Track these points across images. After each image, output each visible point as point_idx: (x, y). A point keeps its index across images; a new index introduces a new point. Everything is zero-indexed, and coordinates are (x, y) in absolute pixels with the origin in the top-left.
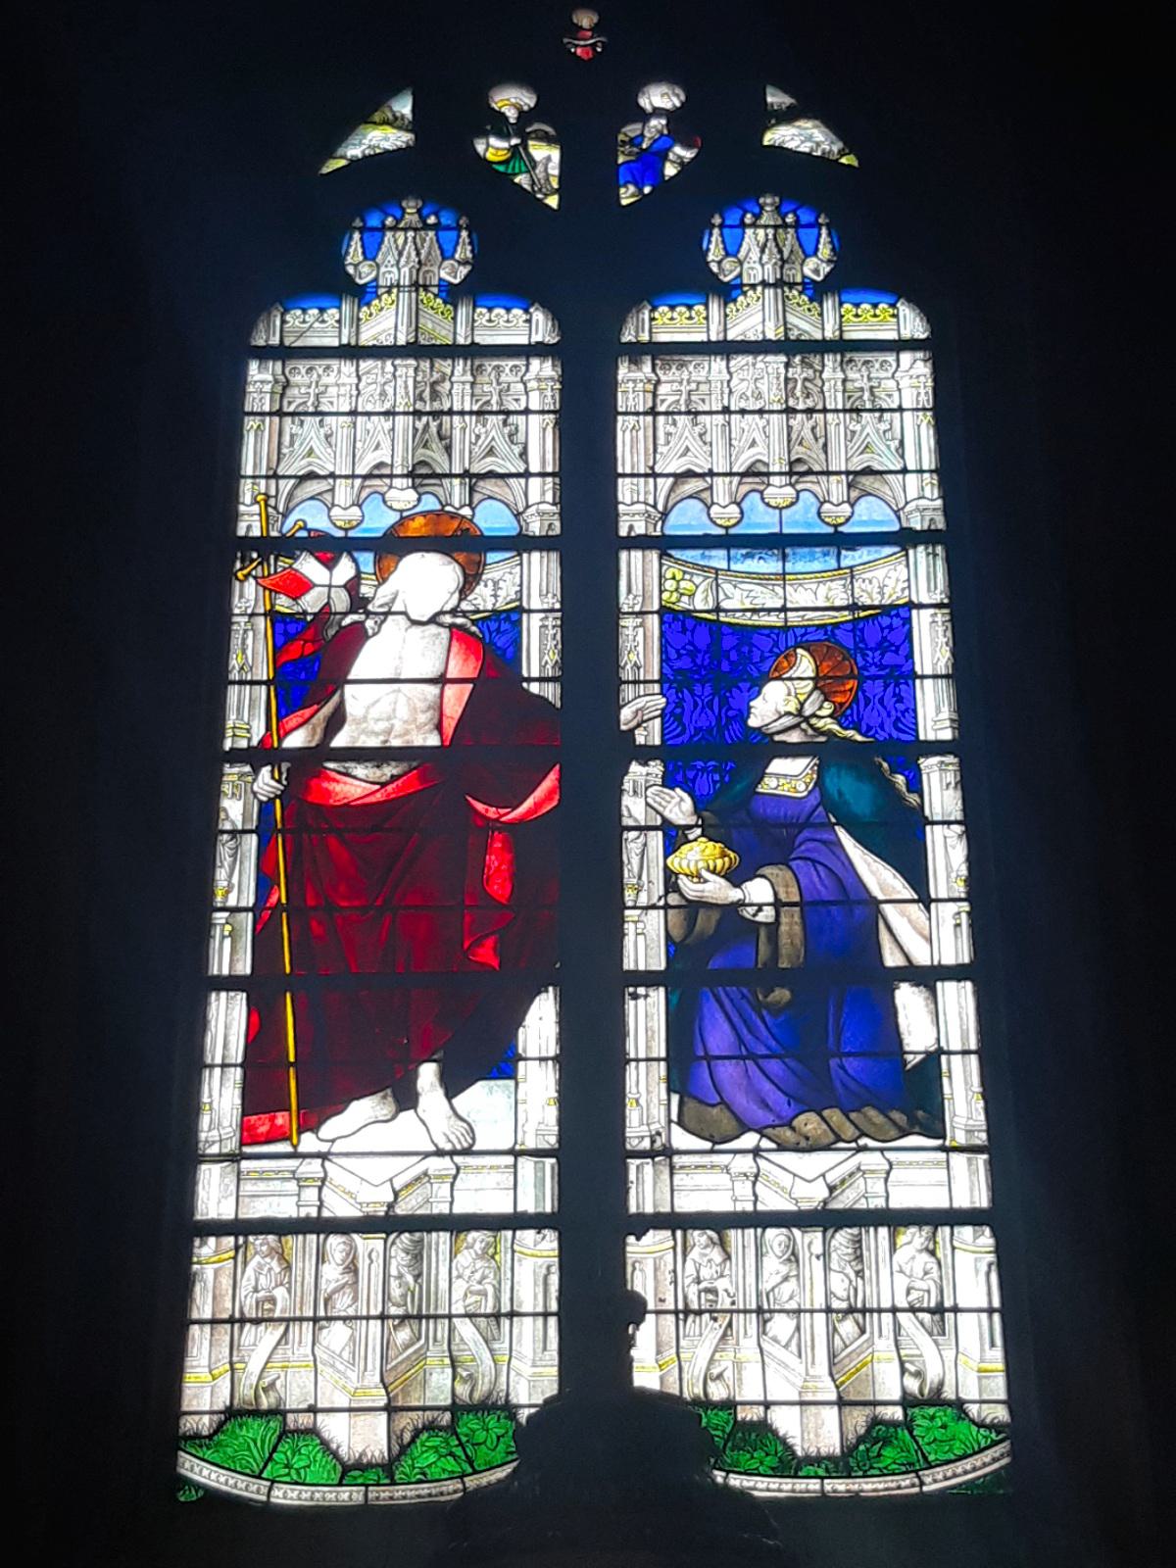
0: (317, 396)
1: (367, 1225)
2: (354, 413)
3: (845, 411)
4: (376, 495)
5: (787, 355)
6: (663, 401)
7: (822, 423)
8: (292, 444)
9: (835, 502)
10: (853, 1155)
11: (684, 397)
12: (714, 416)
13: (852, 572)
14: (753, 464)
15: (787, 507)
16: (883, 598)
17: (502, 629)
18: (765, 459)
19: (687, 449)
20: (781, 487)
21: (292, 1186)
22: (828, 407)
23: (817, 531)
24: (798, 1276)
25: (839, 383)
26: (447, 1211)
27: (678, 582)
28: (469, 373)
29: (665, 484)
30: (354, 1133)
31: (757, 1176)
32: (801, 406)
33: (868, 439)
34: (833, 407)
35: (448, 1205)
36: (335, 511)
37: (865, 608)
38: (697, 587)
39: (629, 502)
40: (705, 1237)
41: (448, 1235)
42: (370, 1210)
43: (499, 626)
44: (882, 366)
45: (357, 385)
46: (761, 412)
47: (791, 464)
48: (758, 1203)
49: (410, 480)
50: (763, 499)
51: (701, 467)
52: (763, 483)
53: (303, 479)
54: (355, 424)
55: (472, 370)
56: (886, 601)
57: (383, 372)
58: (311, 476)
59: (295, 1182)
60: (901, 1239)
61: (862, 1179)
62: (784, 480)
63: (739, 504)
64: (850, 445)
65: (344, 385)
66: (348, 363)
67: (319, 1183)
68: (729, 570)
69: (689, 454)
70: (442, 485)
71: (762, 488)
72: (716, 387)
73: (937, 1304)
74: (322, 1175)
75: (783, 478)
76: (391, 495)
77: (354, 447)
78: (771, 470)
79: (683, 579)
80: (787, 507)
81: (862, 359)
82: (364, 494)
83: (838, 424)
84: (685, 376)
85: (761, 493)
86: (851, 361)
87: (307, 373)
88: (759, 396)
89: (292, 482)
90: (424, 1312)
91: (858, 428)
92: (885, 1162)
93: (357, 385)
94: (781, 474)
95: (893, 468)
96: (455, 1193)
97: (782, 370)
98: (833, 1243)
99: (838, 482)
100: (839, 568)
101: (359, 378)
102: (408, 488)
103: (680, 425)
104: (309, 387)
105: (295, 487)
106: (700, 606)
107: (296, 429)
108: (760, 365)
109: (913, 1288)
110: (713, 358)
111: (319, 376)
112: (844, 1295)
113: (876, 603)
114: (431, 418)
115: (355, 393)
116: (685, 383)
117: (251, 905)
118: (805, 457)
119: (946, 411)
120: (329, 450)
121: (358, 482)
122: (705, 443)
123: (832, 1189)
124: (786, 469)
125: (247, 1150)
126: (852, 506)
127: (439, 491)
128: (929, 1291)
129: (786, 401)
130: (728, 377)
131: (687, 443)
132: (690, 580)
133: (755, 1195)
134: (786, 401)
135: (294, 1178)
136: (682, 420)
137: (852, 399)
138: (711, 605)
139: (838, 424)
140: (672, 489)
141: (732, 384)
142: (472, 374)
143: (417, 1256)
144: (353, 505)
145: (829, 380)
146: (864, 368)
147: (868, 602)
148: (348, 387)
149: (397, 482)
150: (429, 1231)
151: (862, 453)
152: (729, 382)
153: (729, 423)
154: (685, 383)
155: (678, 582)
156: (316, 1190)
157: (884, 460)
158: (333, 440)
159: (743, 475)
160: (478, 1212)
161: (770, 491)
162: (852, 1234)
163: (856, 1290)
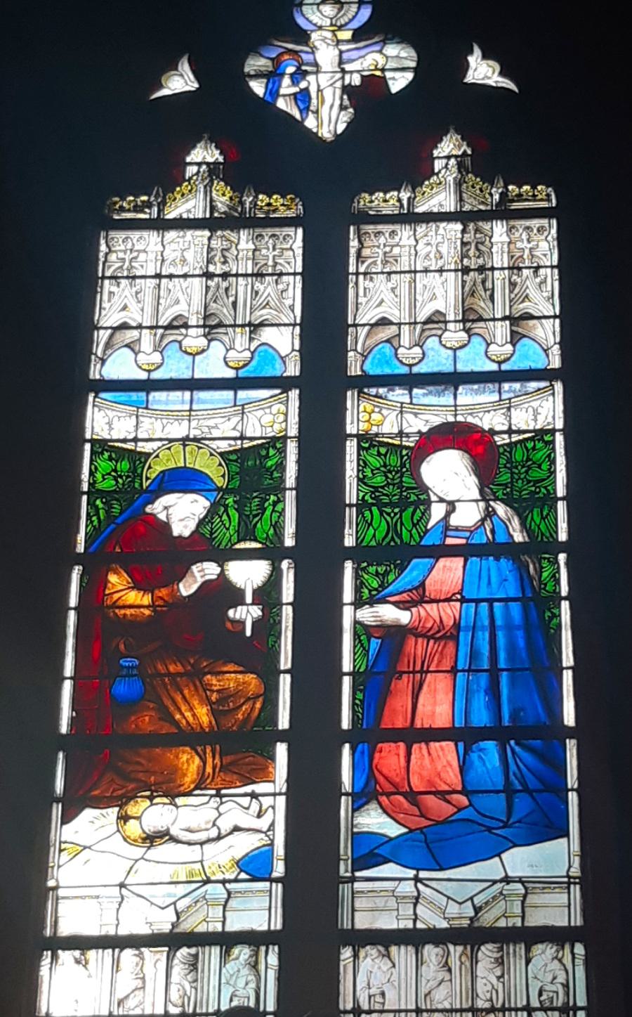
0: (131, 261)
1: (153, 941)
2: (158, 276)
3: (252, 275)
4: (434, 338)
5: (210, 231)
6: (109, 267)
7: (234, 284)
8: (365, 295)
9: (408, 346)
10: (201, 886)
11: (127, 264)
12: (148, 280)
13: (243, 409)
14: (175, 319)
15: (461, 347)
16: (536, 424)
17: (537, 447)
18: (444, 311)
19: (382, 301)
20: (455, 332)
21: (392, 903)
22: (495, 266)
23: (397, 371)
24: (451, 980)
25: (505, 246)
26: (220, 929)
27: (370, 414)
28: (251, 242)
29: (419, 327)
30: (158, 862)
31: (417, 898)
32: (218, 272)
33: (269, 298)
34: (500, 266)
35: (220, 924)
36: (140, 356)
37: (519, 432)
38: (385, 418)
39: (408, 346)
40: (375, 950)
41: (218, 948)
42: (456, 923)
43: (535, 445)
44: (284, 239)
45: (162, 252)
46: (185, 276)
47: (206, 317)
48: (418, 922)
49: (461, 324)
50: (441, 342)
51: (134, 320)
52: (440, 329)
53: (116, 329)
54: (159, 286)
55: (253, 239)
56: (538, 427)
57: (436, 234)
58: (124, 326)
59: (395, 899)
60: (362, 953)
61: (503, 902)
62: (201, 331)
63: (421, 347)
64: (254, 302)
65: (405, 246)
66: (408, 227)
67: (414, 901)
68: (138, 408)
69: (383, 304)
70: (227, 334)
71: (180, 338)
72: (152, 256)
73: (563, 1004)
74: (415, 894)
75: (458, 324)
76: (186, 343)
77: (158, 304)
78: (447, 319)
79: (373, 412)
80: (461, 347)
81: (270, 234)
82: (165, 341)
83: (504, 279)
84: (129, 246)
85: (180, 342)
86: (513, 227)
87: (123, 242)
88: (184, 261)
89: (109, 331)
90: (507, 1006)
91: (262, 288)
92: (225, 892)
93: (162, 252)
94: (197, 326)
95: (546, 314)
96: (227, 914)
97: (459, 235)
98: (480, 954)
99: (502, 326)
100: (243, 405)
101: (417, 241)
102: (460, 330)
103: (122, 286)
104: (125, 253)
105: (111, 336)
106: (386, 429)
107: (114, 289)
108: (441, 231)
109: (236, 996)
110: (151, 233)
111: (133, 245)
112: (179, 1002)
113: (531, 428)
114: (220, 279)
115: (413, 252)
116: (382, 247)
117: (282, 675)
118: (218, 312)
119: (565, 267)
120: (396, 300)
121: (160, 331)
122: (396, 296)
123: (477, 910)
124: (201, 323)
125: (358, 874)
126: (514, 345)
127: (226, 339)
128: (557, 993)
129: (207, 267)
130: (162, 249)
131: (382, 296)
132: (379, 412)
133: (415, 914)
134: (207, 267)
135: (393, 896)
136: (124, 282)
137: (258, 266)
138: (396, 430)
139: (246, 285)
140: (368, 335)
141: (417, 248)
142: (254, 243)
143: (193, 965)
144: (416, 345)
145: (243, 250)
146: (271, 241)
147: (524, 427)
148: (407, 248)
149: (192, 332)
150: (203, 945)
151: (378, 306)
152: (415, 246)
153: (415, 281)
154: (382, 247)
155: (370, 414)
156: (412, 906)
157: (541, 308)
158: (397, 292)
159: (166, 328)
160: (135, 932)
161: (447, 334)
162: (189, 954)
163: (189, 998)
